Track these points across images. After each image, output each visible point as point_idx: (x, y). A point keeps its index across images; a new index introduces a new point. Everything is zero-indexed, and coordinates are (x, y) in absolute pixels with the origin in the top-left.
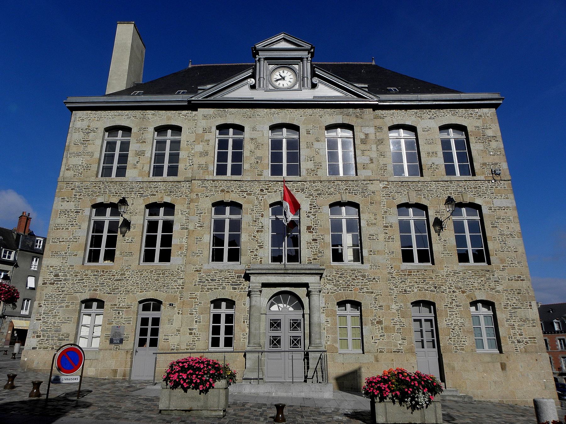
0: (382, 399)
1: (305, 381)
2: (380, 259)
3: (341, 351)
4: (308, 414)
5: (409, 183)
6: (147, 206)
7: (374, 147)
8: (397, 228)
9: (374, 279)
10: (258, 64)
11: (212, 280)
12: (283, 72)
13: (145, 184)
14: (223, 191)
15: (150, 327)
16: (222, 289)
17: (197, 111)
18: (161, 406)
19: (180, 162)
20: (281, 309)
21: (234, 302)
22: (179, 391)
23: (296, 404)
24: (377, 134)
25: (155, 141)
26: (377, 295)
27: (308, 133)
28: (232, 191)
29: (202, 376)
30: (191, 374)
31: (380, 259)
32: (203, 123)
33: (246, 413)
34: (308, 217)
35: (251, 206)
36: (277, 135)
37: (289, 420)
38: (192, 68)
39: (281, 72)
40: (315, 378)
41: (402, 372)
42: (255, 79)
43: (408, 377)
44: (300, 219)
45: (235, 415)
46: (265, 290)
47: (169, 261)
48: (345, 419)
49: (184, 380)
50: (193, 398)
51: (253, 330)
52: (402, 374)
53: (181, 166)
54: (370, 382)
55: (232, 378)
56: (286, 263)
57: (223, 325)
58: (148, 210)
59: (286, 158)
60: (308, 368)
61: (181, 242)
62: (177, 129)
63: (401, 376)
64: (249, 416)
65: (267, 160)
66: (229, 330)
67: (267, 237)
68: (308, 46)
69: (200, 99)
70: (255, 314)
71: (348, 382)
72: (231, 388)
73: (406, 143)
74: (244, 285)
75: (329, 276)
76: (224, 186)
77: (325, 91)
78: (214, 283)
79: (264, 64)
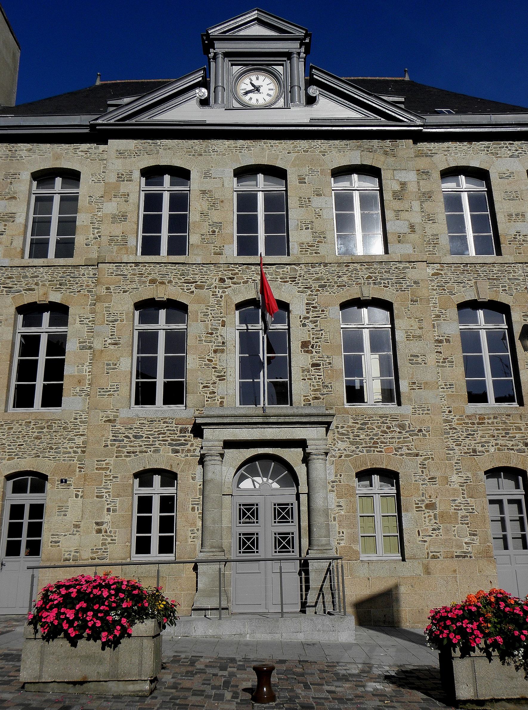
0: (466, 651)
1: (303, 611)
2: (430, 397)
3: (363, 557)
4: (316, 679)
5: (478, 267)
6: (20, 310)
7: (416, 205)
8: (457, 343)
9: (420, 431)
10: (213, 64)
11: (135, 437)
12: (257, 79)
13: (15, 271)
14: (153, 281)
15: (26, 521)
16: (154, 451)
17: (106, 143)
18: (25, 676)
19: (78, 231)
20: (257, 486)
21: (176, 475)
22: (60, 644)
23: (291, 656)
24: (422, 183)
25: (33, 197)
26: (425, 459)
27: (302, 181)
28: (170, 282)
29: (107, 613)
30: (84, 611)
31: (430, 397)
32: (117, 165)
33: (196, 683)
34: (304, 325)
35: (203, 307)
36: (247, 186)
37: (282, 695)
38: (101, 86)
39: (254, 78)
40: (320, 605)
41: (502, 598)
42: (208, 87)
43: (518, 608)
44: (289, 329)
45: (175, 686)
46: (229, 453)
47: (61, 406)
48: (389, 688)
49: (70, 623)
50: (88, 658)
51: (209, 523)
52: (505, 602)
53: (79, 239)
54: (440, 618)
55: (168, 614)
56: (266, 405)
57: (156, 514)
58: (21, 317)
59: (263, 224)
60: (307, 588)
61: (79, 371)
62: (72, 176)
63: (502, 605)
64: (202, 688)
65: (232, 229)
66: (167, 524)
67: (232, 360)
68: (300, 33)
69: (112, 122)
70: (212, 494)
71: (378, 612)
72: (169, 631)
73: (470, 198)
74: (192, 445)
75: (342, 427)
76: (155, 272)
77: (329, 110)
78: (138, 442)
79: (223, 64)
